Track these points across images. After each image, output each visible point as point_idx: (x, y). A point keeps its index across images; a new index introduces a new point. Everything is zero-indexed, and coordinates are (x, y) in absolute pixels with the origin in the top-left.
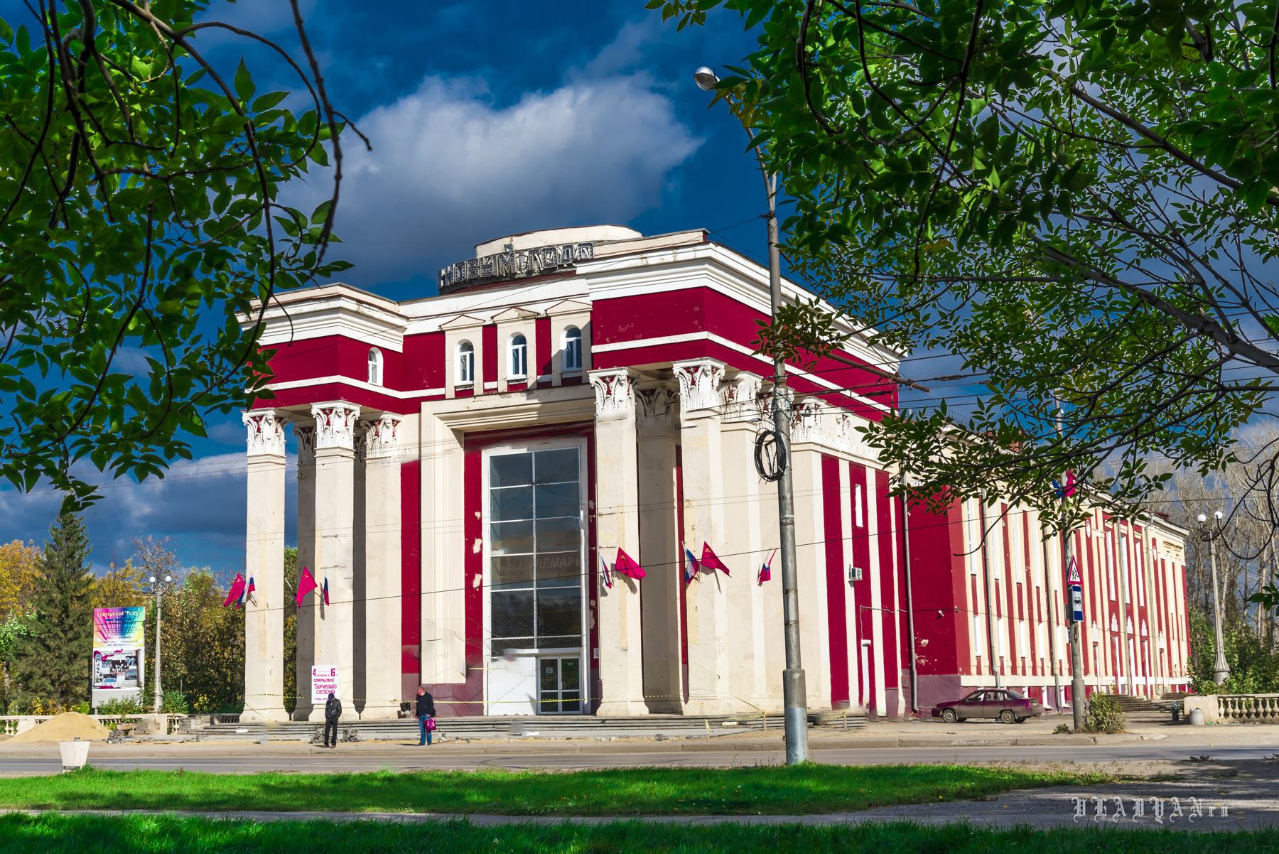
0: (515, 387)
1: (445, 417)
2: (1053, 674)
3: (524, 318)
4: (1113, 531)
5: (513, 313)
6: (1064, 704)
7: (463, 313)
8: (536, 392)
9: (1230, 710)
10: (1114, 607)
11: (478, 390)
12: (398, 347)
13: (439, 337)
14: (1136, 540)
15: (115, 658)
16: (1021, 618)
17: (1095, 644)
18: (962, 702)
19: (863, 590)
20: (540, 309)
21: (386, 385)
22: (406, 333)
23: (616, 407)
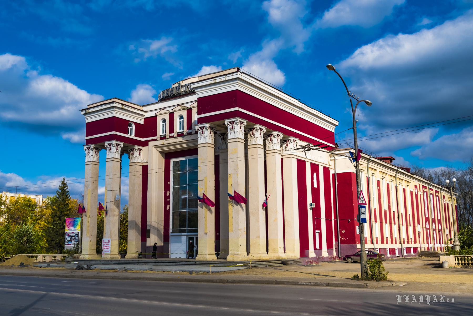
0: (180, 135)
1: (156, 147)
2: (400, 243)
3: (183, 109)
4: (427, 192)
5: (179, 108)
6: (405, 254)
7: (162, 109)
8: (186, 137)
9: (460, 262)
10: (427, 219)
11: (167, 137)
12: (142, 122)
13: (155, 118)
14: (436, 196)
15: (71, 235)
16: (386, 222)
17: (419, 233)
18: (354, 255)
19: (316, 212)
20: (188, 105)
21: (135, 136)
22: (145, 117)
23: (206, 138)
